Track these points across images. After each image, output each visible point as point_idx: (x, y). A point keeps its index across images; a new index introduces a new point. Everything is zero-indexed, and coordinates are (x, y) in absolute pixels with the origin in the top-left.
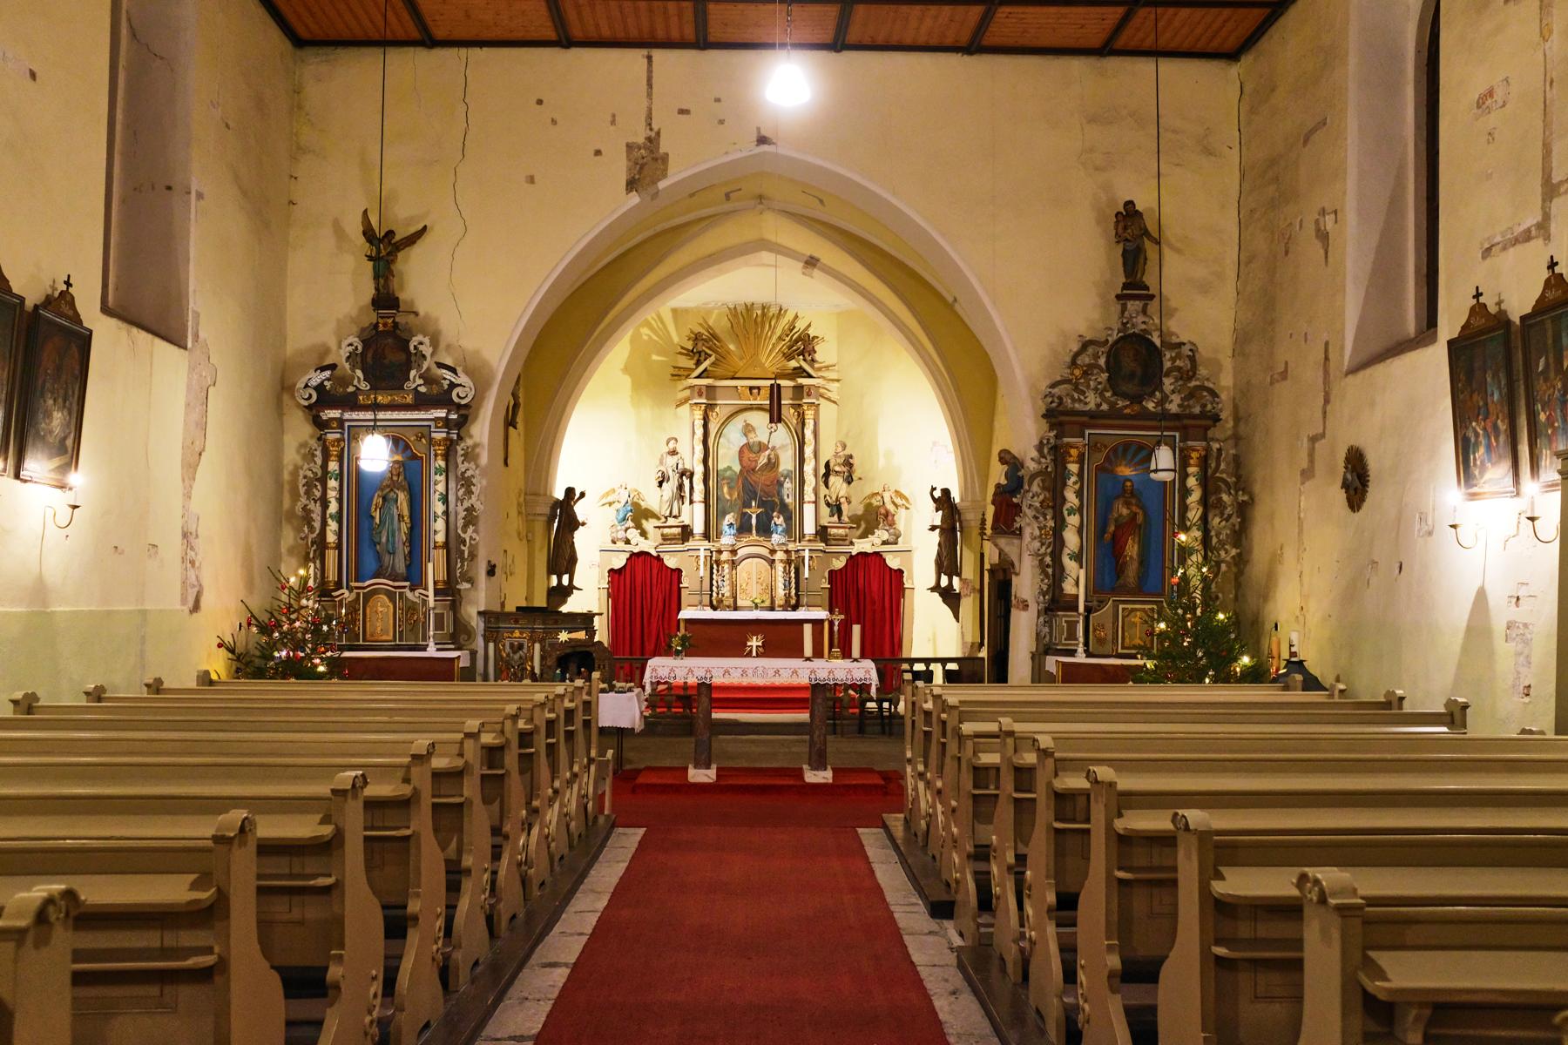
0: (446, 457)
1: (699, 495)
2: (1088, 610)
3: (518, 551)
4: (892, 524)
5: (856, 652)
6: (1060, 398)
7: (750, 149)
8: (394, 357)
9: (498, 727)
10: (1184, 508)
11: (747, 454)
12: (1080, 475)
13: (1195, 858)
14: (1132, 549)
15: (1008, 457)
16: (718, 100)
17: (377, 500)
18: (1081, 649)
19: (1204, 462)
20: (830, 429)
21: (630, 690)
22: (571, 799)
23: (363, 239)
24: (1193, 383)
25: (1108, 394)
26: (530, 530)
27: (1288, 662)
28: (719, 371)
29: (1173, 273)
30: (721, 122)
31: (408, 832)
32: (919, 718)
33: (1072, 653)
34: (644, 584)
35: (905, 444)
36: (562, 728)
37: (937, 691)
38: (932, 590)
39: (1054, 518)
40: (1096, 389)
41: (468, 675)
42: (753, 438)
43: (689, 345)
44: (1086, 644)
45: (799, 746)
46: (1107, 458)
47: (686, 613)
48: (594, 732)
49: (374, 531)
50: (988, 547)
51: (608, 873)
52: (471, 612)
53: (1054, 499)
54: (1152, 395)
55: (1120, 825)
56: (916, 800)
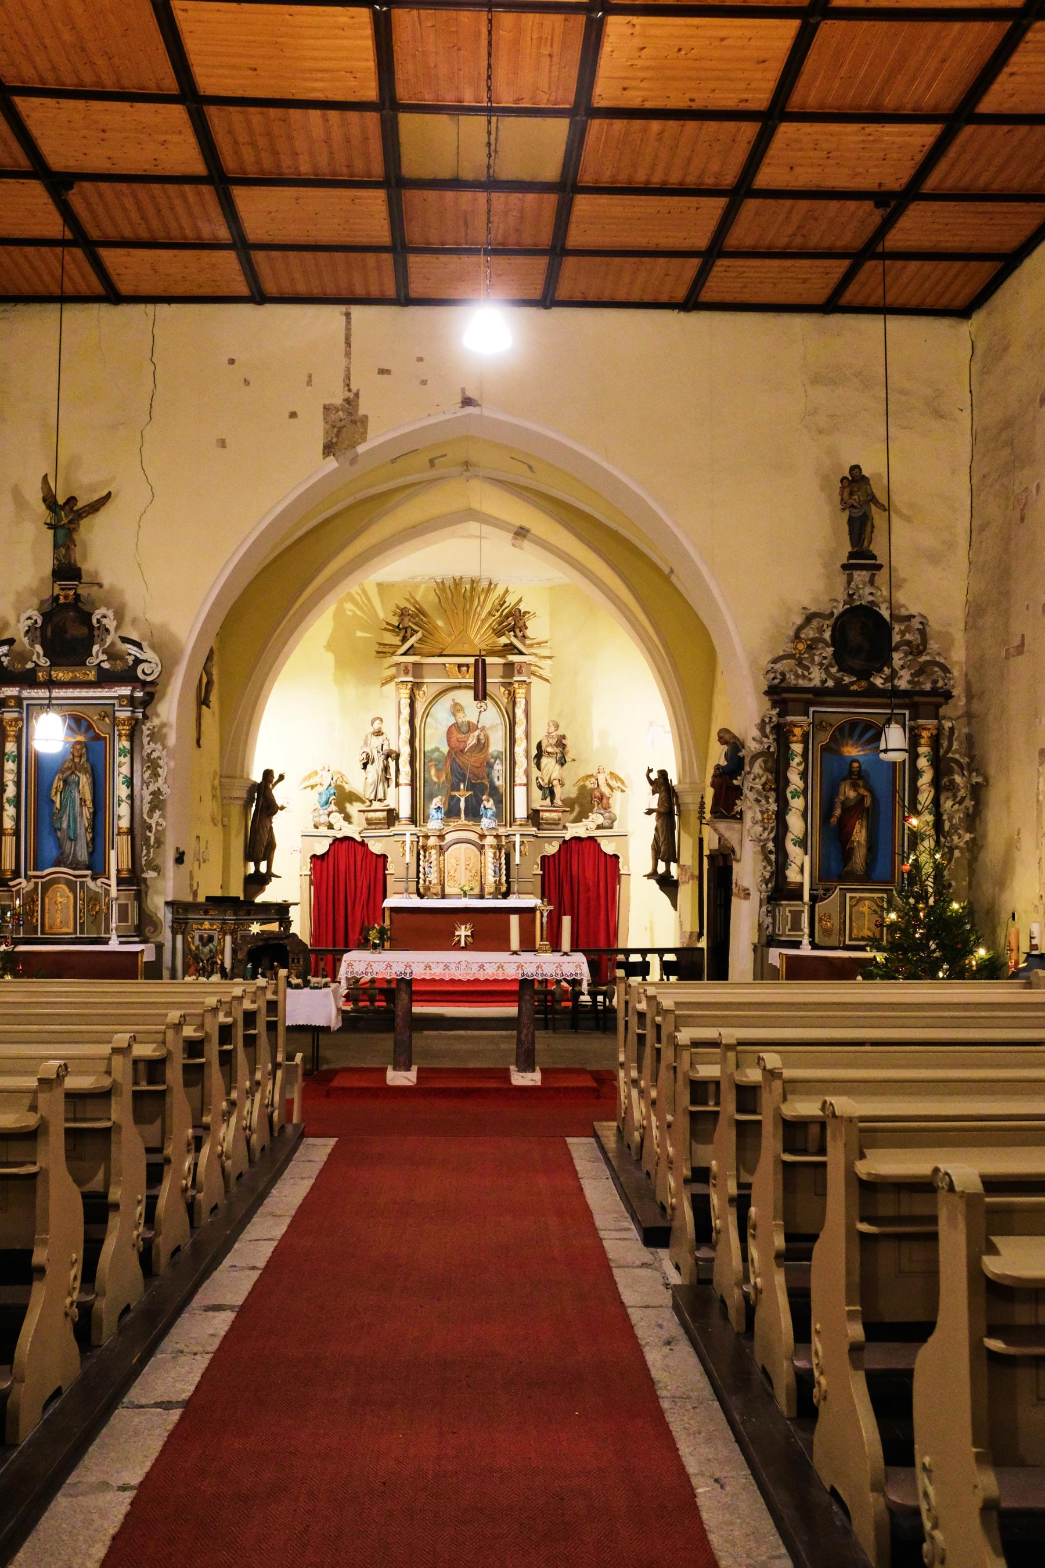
0: (131, 737)
1: (405, 777)
2: (814, 899)
3: (213, 836)
4: (607, 808)
5: (566, 945)
6: (783, 674)
7: (454, 411)
8: (78, 631)
9: (160, 1037)
10: (915, 791)
11: (456, 735)
12: (805, 755)
13: (962, 1226)
14: (860, 834)
15: (727, 737)
16: (420, 359)
17: (57, 783)
18: (806, 941)
19: (935, 743)
20: (542, 709)
21: (326, 985)
22: (252, 1111)
23: (44, 507)
24: (924, 658)
25: (834, 670)
26: (226, 815)
27: (1029, 955)
28: (426, 648)
29: (901, 541)
30: (424, 382)
31: (33, 1169)
32: (634, 1021)
33: (797, 945)
34: (348, 869)
35: (619, 725)
36: (239, 1032)
37: (651, 991)
38: (649, 876)
39: (777, 801)
40: (821, 664)
41: (153, 971)
42: (462, 718)
43: (395, 621)
44: (812, 935)
45: (506, 1041)
46: (833, 738)
47: (391, 902)
48: (281, 1030)
49: (55, 816)
50: (707, 832)
51: (291, 1191)
52: (158, 903)
53: (777, 781)
54: (880, 670)
55: (864, 1168)
56: (629, 1108)
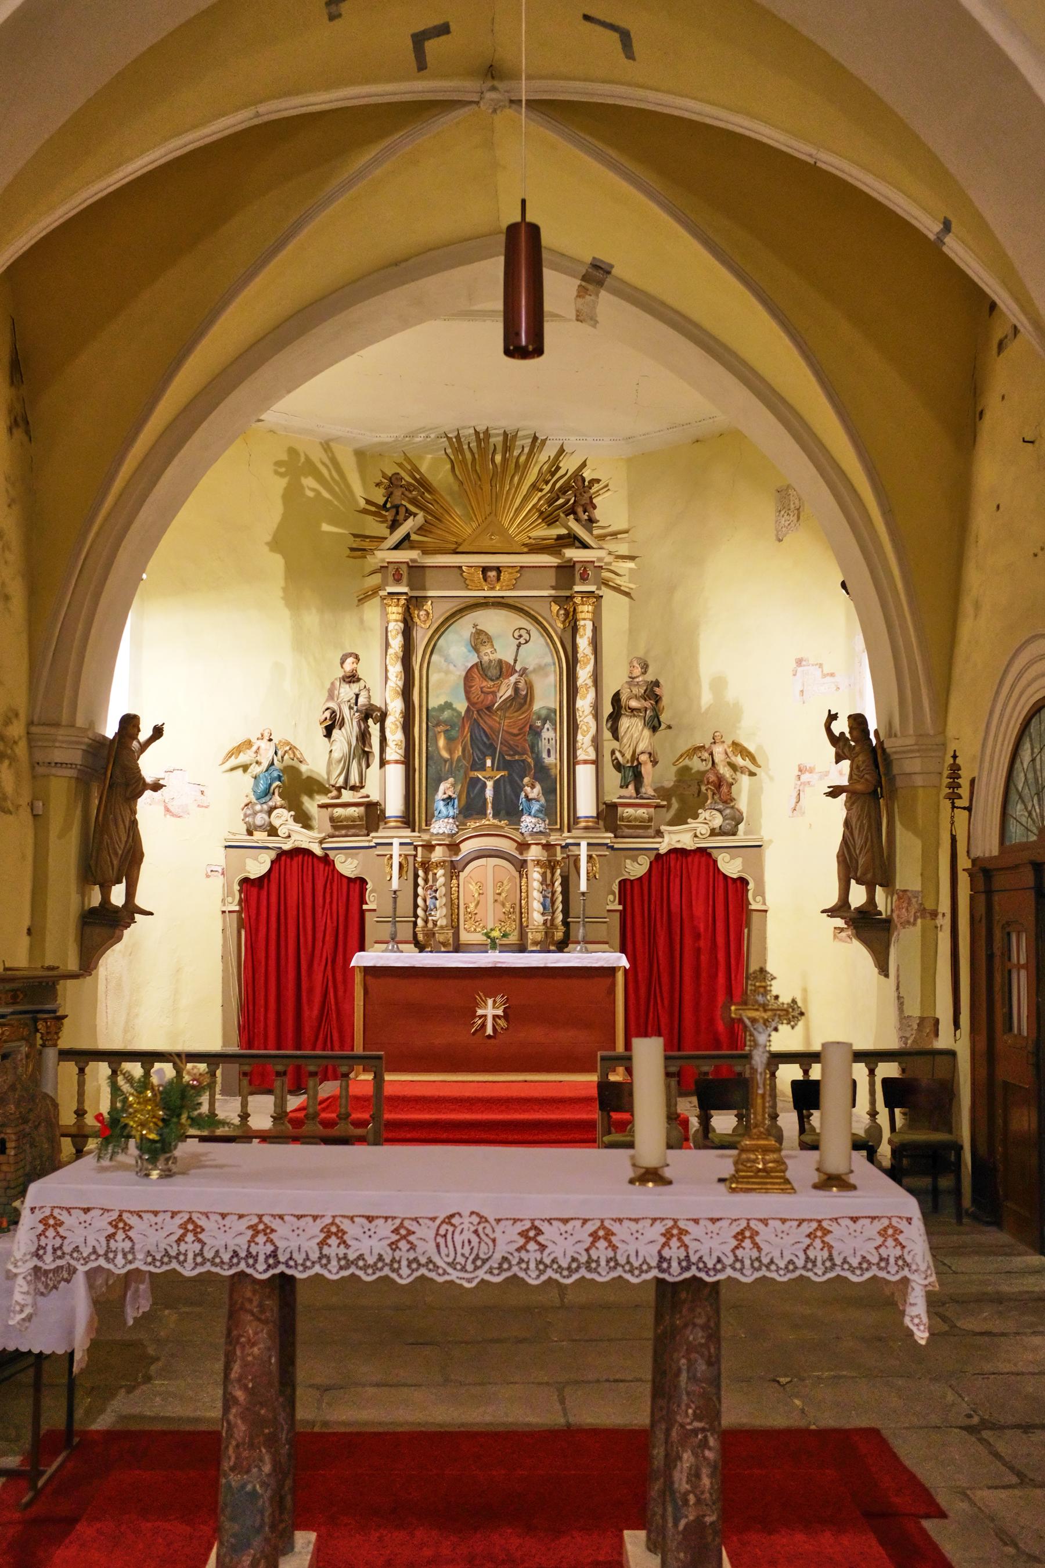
1: (394, 752)
4: (728, 800)
11: (479, 683)
38: (832, 912)
42: (489, 655)
